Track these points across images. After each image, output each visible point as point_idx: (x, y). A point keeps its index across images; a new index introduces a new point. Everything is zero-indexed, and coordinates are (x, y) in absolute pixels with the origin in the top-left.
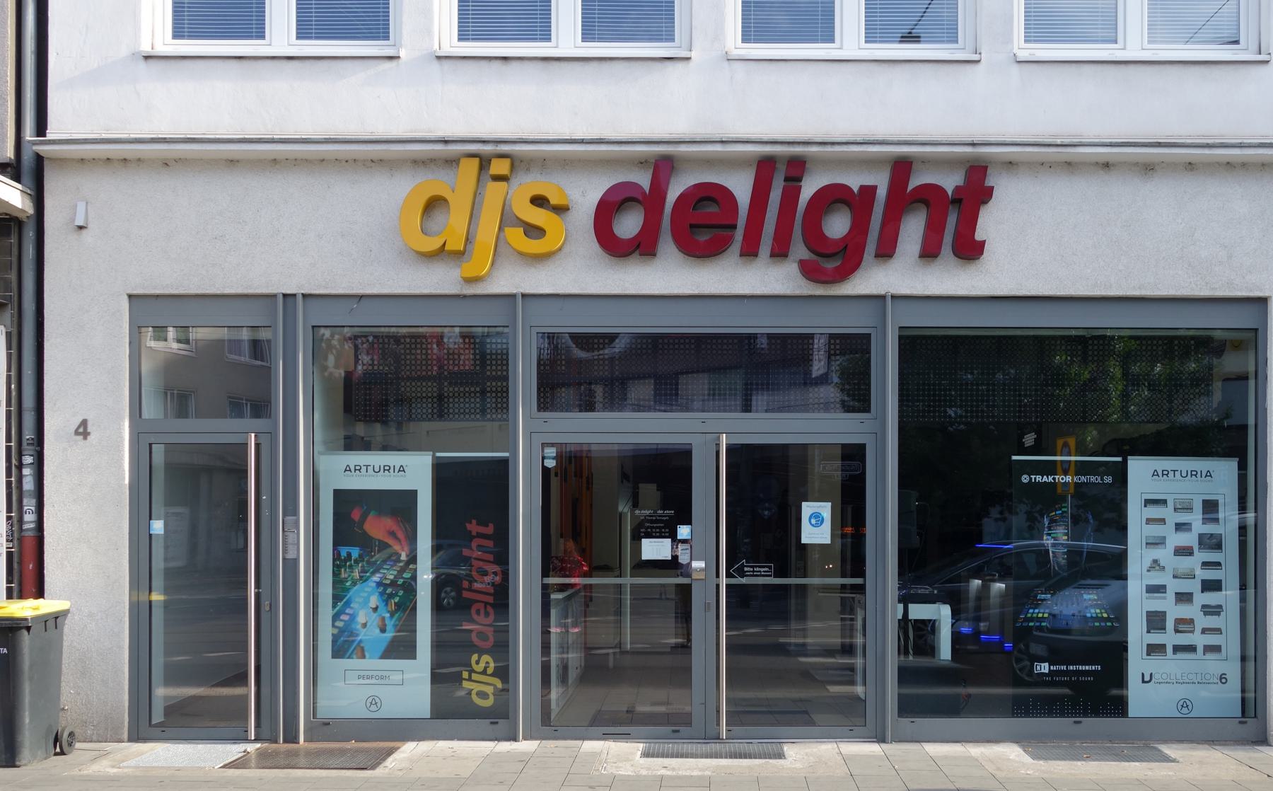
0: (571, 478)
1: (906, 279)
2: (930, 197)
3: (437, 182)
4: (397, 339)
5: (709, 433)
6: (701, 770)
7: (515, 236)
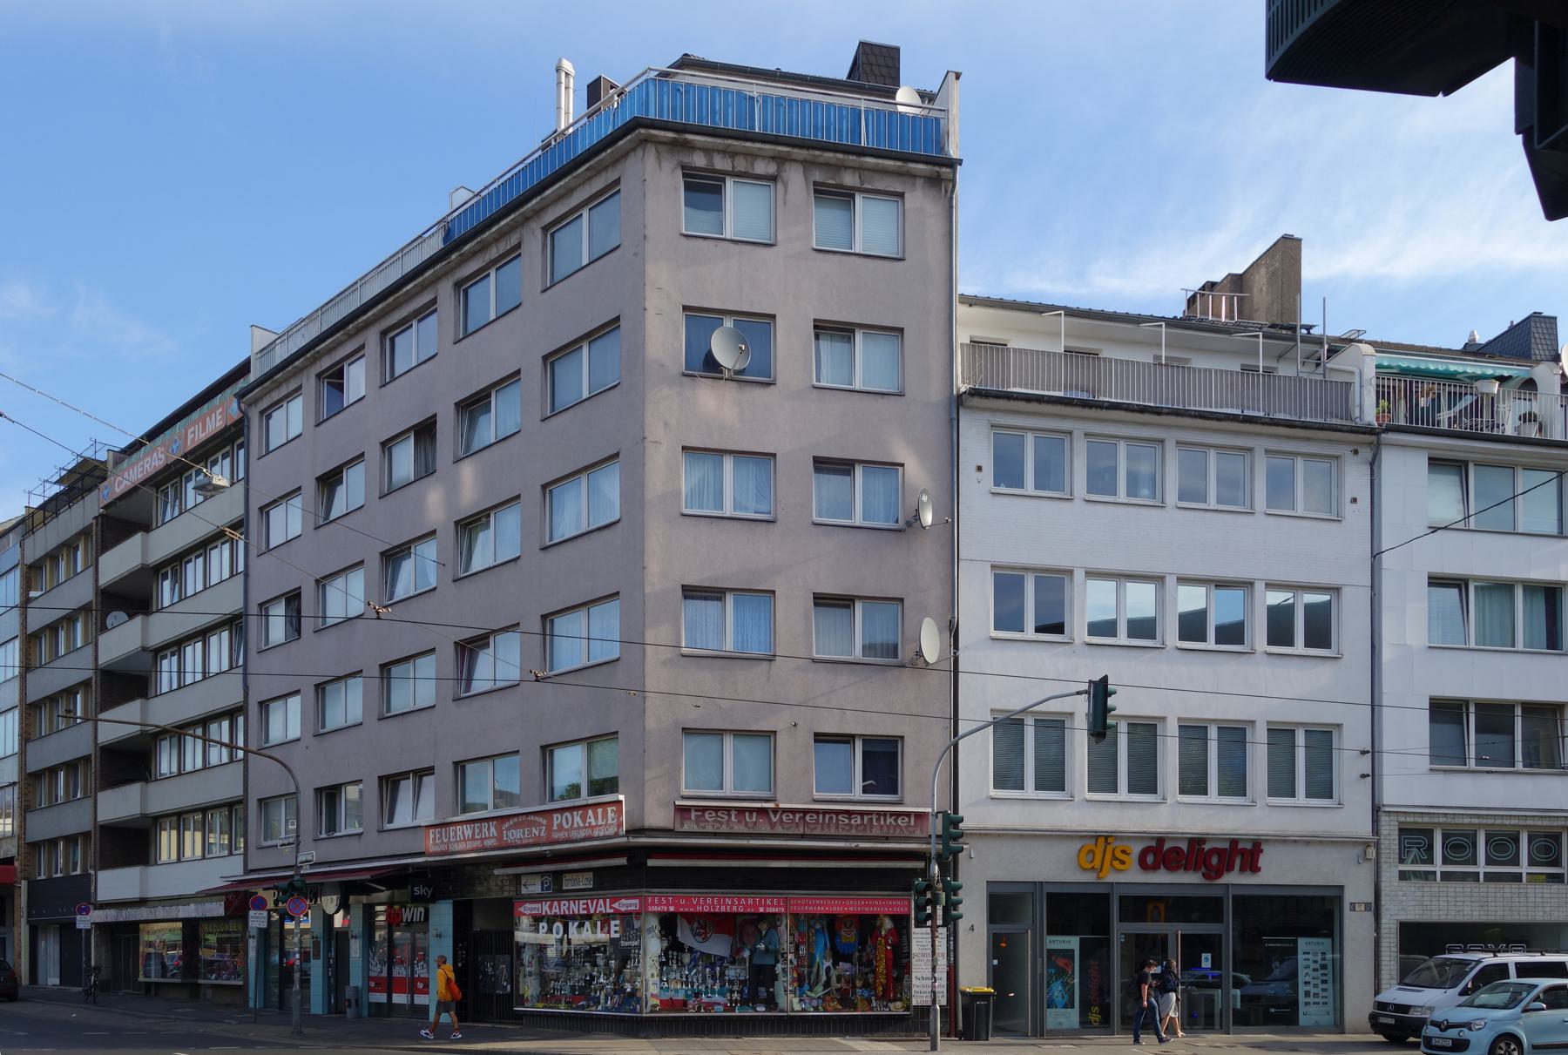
1: (1233, 878)
2: (1243, 852)
7: (1116, 863)
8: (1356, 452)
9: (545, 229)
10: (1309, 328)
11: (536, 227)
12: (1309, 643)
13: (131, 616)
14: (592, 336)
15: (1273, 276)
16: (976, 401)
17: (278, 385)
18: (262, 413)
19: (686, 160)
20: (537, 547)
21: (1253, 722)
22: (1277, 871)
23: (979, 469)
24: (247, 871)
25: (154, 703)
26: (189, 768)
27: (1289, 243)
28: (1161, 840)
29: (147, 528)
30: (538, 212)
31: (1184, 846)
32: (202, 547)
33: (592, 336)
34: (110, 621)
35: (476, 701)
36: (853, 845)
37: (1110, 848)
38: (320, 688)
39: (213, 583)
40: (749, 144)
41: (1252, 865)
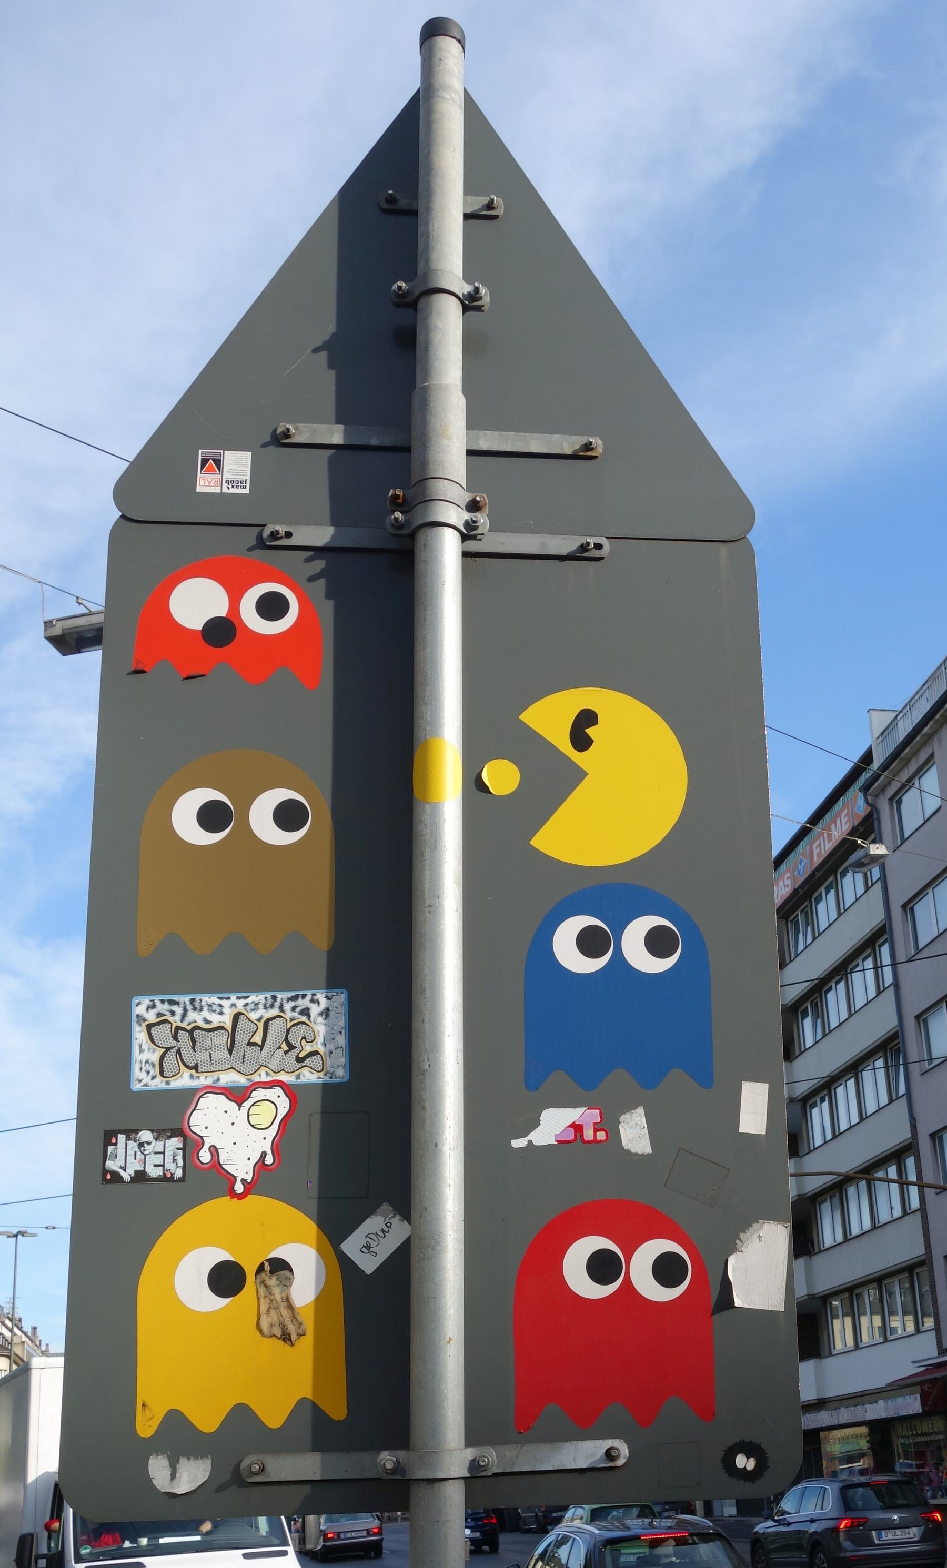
32: (842, 970)
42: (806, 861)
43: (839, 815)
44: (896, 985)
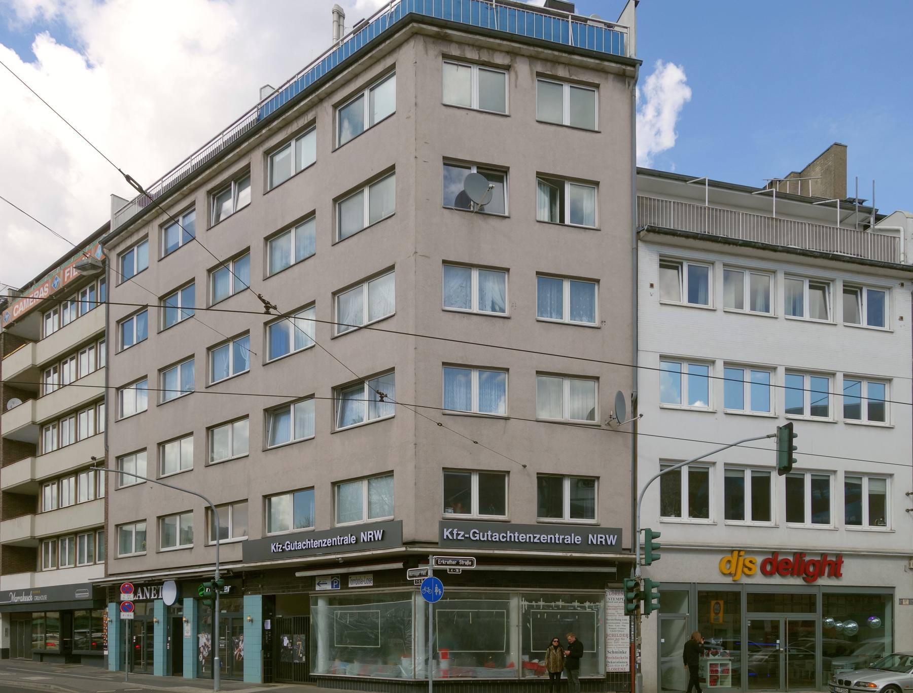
0: (756, 626)
1: (825, 581)
2: (830, 563)
3: (728, 557)
4: (833, 595)
5: (782, 618)
6: (551, 606)
7: (746, 570)
8: (902, 285)
9: (335, 107)
10: (861, 202)
11: (328, 106)
12: (871, 418)
13: (24, 401)
14: (372, 181)
15: (827, 171)
16: (652, 236)
17: (131, 235)
18: (119, 255)
19: (446, 50)
20: (329, 338)
21: (835, 472)
22: (854, 576)
23: (652, 286)
24: (107, 575)
25: (40, 461)
26: (65, 504)
27: (839, 148)
28: (775, 554)
29: (36, 341)
30: (330, 94)
31: (791, 559)
32: (75, 352)
33: (372, 181)
34: (9, 406)
35: (281, 452)
36: (569, 554)
37: (741, 559)
38: (162, 445)
39: (81, 379)
40: (491, 40)
41: (836, 572)
42: (60, 280)
43: (43, 286)
44: (107, 367)
